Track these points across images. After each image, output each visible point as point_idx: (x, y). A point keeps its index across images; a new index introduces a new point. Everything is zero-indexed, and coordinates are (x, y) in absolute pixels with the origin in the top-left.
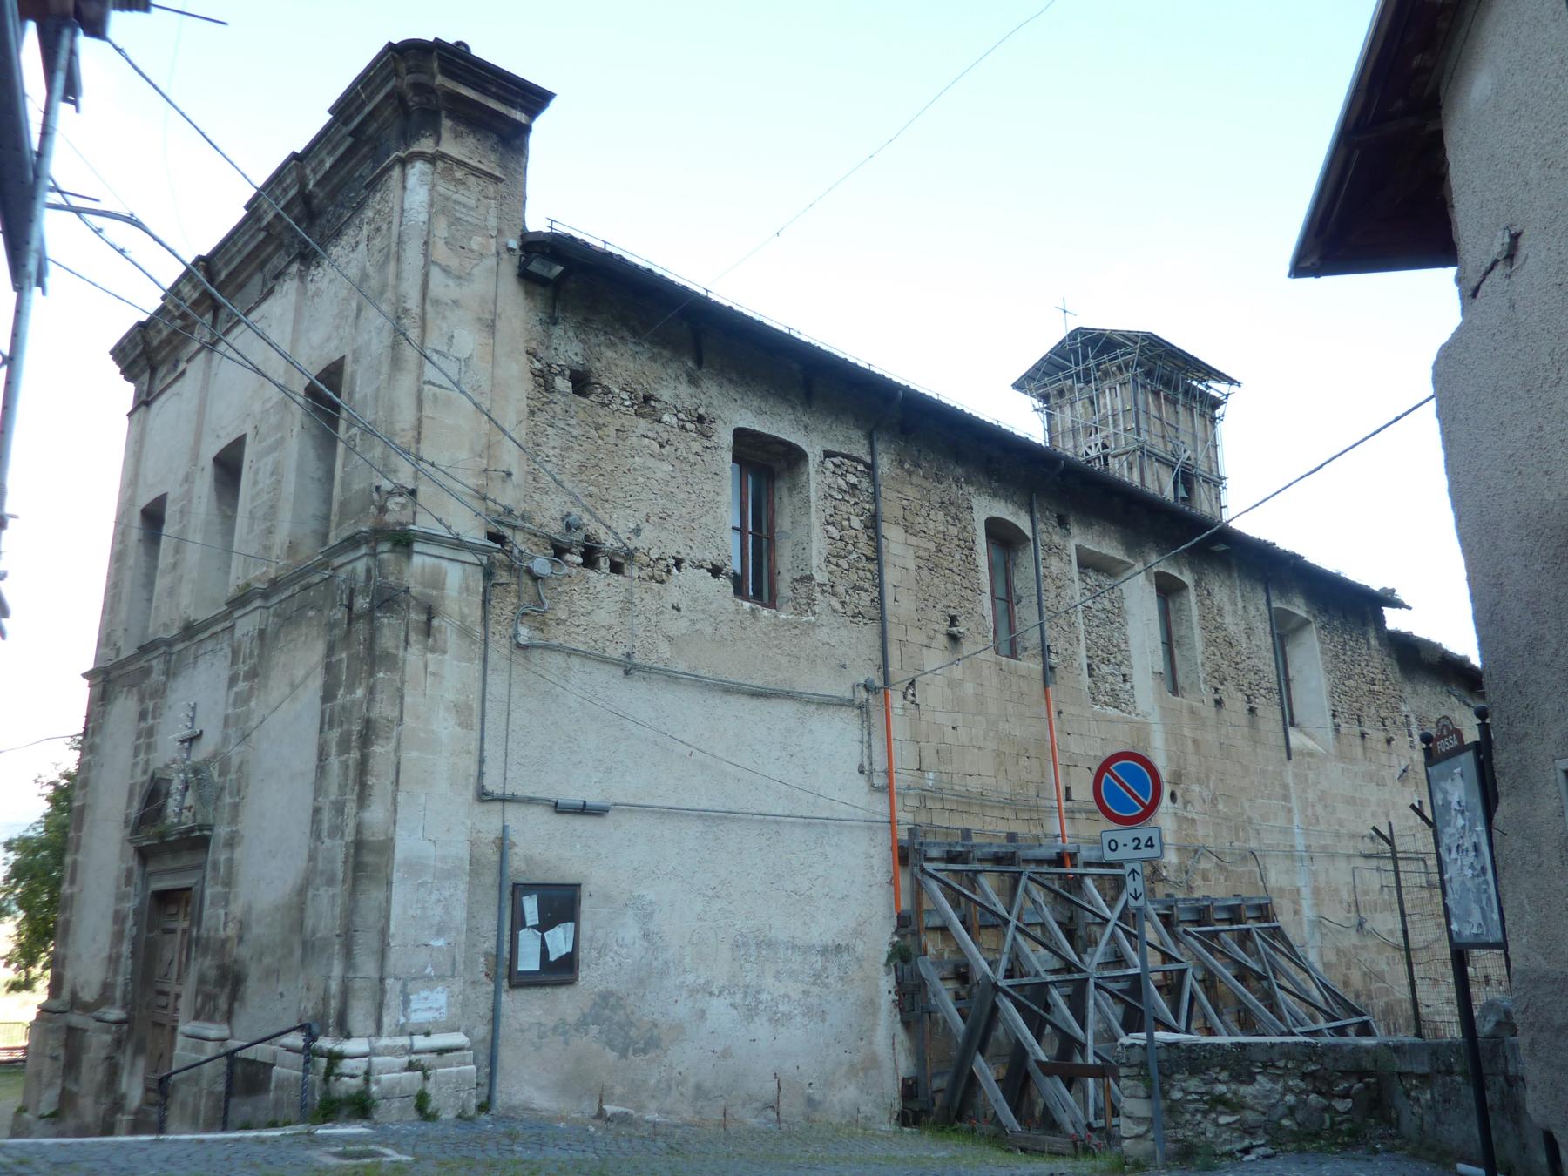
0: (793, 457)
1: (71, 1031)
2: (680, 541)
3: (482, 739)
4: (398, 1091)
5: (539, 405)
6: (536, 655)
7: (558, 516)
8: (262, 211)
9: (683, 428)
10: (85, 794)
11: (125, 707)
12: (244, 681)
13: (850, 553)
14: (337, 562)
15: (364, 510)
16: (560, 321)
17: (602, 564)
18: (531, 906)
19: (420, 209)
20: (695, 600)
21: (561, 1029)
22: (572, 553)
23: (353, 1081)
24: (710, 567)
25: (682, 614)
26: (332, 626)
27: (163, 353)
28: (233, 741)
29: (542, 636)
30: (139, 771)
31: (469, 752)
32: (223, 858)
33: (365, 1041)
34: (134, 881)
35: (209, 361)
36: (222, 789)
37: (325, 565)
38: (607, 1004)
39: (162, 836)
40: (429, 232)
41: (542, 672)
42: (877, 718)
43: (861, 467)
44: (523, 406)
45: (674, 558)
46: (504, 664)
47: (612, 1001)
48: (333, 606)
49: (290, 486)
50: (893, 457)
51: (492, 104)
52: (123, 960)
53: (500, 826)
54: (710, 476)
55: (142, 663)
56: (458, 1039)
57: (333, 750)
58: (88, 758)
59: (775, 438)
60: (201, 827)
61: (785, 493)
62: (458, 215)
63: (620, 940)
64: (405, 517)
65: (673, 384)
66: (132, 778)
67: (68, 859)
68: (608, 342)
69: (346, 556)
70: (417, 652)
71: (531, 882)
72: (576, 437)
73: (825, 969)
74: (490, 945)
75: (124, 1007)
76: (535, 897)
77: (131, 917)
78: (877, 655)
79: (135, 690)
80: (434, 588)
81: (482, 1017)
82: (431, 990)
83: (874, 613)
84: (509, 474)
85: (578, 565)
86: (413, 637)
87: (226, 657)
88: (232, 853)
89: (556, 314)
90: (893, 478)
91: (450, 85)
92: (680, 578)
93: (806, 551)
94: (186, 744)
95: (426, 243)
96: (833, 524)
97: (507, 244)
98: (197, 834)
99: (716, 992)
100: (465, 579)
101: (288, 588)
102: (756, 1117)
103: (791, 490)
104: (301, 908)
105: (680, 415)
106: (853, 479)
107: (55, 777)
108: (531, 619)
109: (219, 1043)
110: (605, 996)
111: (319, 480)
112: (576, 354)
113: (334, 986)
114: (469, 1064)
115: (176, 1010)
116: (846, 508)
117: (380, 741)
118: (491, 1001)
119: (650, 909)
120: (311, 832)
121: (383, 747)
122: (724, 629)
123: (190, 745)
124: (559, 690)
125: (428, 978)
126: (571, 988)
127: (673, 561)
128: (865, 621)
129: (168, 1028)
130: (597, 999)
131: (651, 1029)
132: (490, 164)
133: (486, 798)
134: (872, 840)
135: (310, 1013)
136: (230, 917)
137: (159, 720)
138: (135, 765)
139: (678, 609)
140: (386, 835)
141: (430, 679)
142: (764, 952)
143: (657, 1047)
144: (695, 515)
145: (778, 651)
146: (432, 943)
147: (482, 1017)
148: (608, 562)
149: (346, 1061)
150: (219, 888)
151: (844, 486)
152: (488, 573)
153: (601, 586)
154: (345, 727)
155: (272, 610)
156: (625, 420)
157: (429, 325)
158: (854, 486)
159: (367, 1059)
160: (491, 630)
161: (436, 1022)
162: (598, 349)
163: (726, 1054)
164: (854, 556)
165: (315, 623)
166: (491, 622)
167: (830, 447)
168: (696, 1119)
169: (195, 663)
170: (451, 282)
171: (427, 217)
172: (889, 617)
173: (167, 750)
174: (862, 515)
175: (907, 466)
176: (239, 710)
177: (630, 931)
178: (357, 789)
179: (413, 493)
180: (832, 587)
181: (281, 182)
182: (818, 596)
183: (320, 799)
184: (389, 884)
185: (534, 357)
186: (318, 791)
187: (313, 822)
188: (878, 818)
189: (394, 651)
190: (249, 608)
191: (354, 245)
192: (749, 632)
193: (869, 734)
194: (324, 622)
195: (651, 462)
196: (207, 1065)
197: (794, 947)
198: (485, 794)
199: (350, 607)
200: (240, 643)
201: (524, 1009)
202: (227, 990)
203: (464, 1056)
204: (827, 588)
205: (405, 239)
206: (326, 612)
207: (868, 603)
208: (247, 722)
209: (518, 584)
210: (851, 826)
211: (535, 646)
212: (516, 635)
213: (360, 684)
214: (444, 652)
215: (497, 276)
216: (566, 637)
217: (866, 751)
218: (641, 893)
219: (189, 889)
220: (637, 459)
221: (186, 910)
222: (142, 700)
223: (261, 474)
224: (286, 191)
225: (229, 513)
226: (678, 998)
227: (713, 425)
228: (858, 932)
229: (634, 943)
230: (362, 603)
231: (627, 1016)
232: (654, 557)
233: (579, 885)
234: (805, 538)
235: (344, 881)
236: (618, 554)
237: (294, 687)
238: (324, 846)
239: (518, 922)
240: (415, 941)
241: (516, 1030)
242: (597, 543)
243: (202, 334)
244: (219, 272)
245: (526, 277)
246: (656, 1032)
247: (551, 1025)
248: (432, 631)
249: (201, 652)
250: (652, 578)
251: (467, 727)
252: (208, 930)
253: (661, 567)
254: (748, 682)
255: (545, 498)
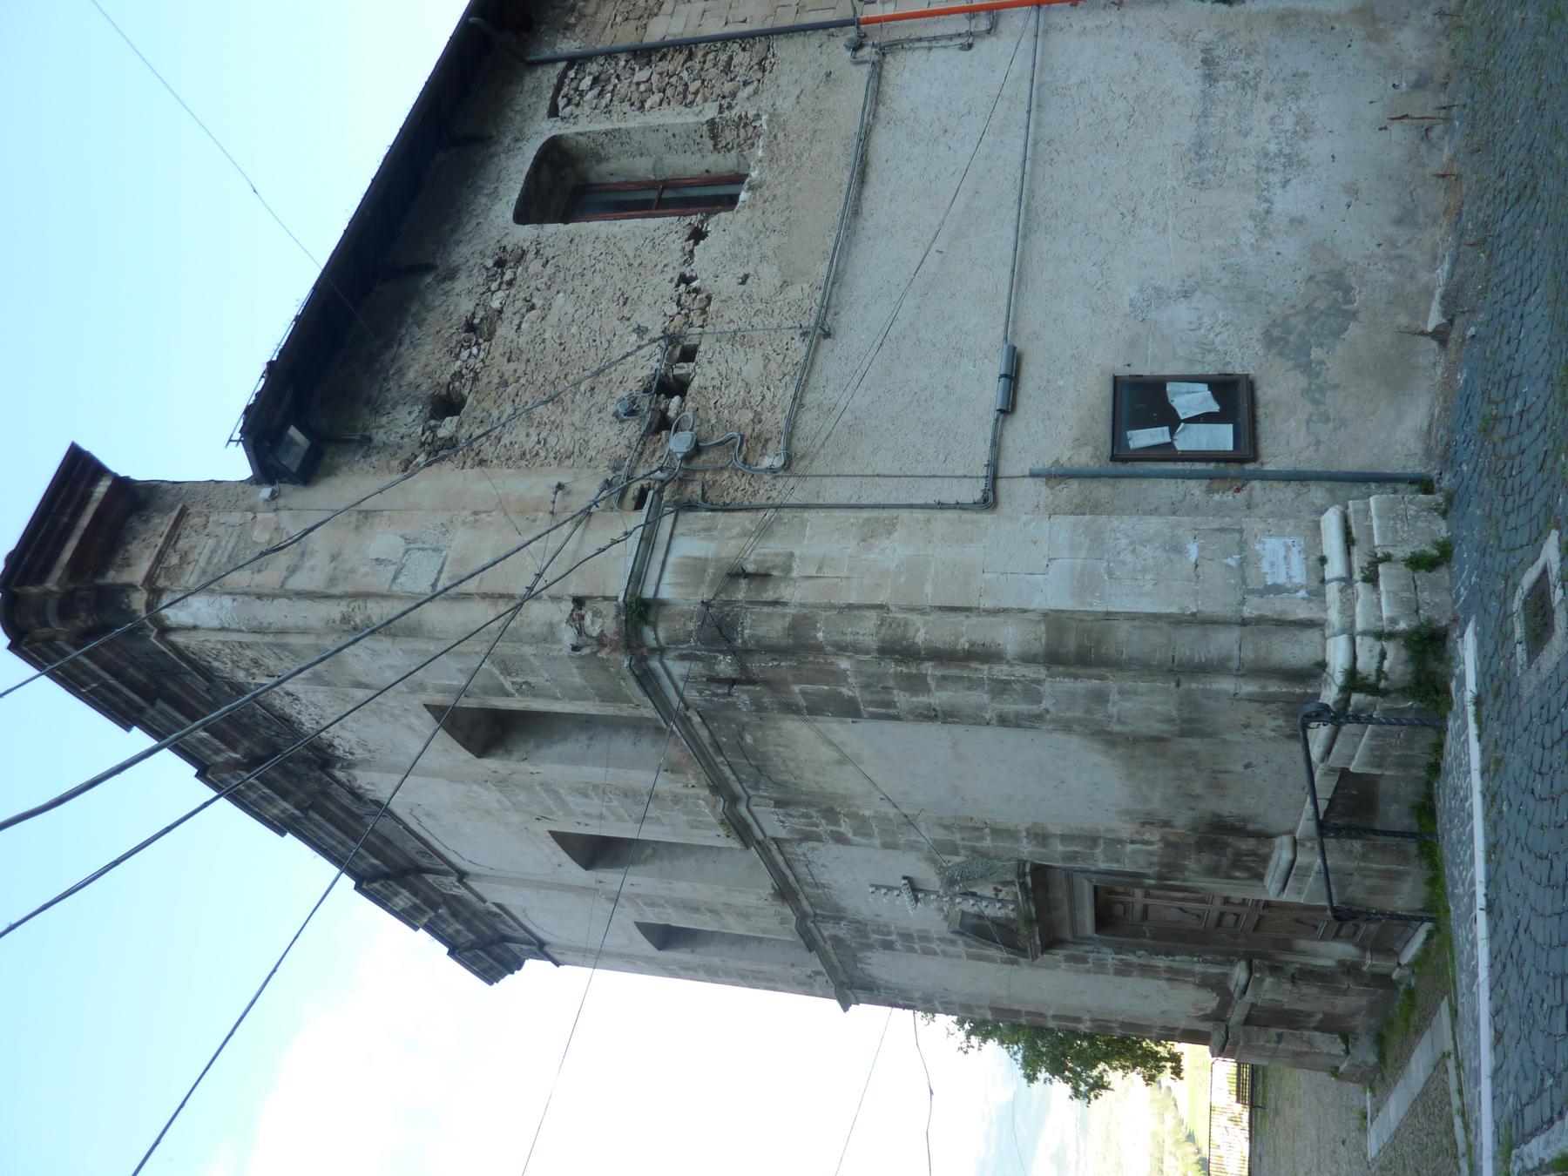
0: (555, 155)
1: (1248, 1021)
2: (656, 280)
3: (910, 506)
4: (1407, 594)
5: (472, 454)
6: (799, 445)
7: (617, 426)
8: (283, 816)
9: (510, 283)
10: (979, 1007)
11: (878, 965)
12: (840, 826)
13: (681, 79)
14: (675, 700)
15: (604, 666)
16: (367, 433)
17: (683, 372)
18: (1141, 438)
19: (217, 605)
20: (735, 257)
21: (1316, 392)
22: (667, 409)
23: (1390, 656)
24: (692, 242)
25: (752, 273)
26: (759, 708)
27: (483, 928)
28: (913, 838)
29: (774, 441)
30: (951, 949)
31: (928, 520)
32: (1060, 848)
33: (1330, 644)
34: (1082, 953)
35: (478, 876)
36: (974, 850)
37: (685, 720)
38: (1282, 339)
39: (1029, 922)
40: (246, 594)
41: (823, 436)
42: (899, 31)
43: (572, 74)
44: (472, 473)
45: (678, 286)
46: (811, 484)
47: (1276, 333)
48: (733, 706)
49: (595, 773)
50: (560, 36)
51: (85, 521)
52: (1175, 965)
53: (1030, 480)
54: (573, 249)
55: (828, 947)
56: (1331, 523)
57: (922, 699)
58: (937, 1004)
59: (529, 176)
60: (1021, 875)
61: (604, 168)
62: (224, 559)
63: (1192, 327)
64: (609, 610)
65: (453, 299)
66: (959, 957)
67: (1051, 1024)
68: (396, 377)
69: (666, 690)
70: (790, 590)
71: (1109, 439)
72: (516, 410)
73: (1235, 77)
74: (1196, 488)
75: (1232, 964)
76: (1130, 433)
77: (1124, 957)
78: (816, 38)
79: (860, 955)
80: (704, 571)
81: (1299, 495)
82: (1259, 558)
83: (759, 47)
84: (560, 487)
85: (683, 401)
86: (770, 595)
87: (814, 849)
88: (1055, 835)
89: (358, 438)
90: (586, 36)
91: (57, 572)
92: (704, 277)
93: (677, 132)
94: (920, 895)
95: (260, 597)
96: (643, 102)
97: (266, 500)
98: (1029, 879)
99: (1266, 205)
100: (693, 533)
101: (721, 771)
102: (1441, 150)
103: (600, 159)
104: (1134, 741)
105: (493, 288)
106: (588, 81)
107: (962, 1035)
108: (752, 453)
109: (1298, 847)
110: (1270, 341)
111: (591, 738)
112: (410, 413)
113: (1249, 687)
114: (1368, 504)
115: (1244, 902)
116: (623, 88)
117: (910, 634)
118: (1275, 484)
119: (1150, 291)
120: (1033, 727)
121: (918, 630)
122: (774, 221)
123: (921, 890)
124: (847, 416)
125: (1243, 562)
126: (1258, 384)
127: (683, 286)
128: (770, 56)
129: (1265, 913)
130: (1273, 351)
131: (1317, 283)
132: (163, 524)
133: (991, 499)
134: (1061, 29)
135: (1280, 722)
136: (1136, 837)
137: (893, 928)
138: (945, 954)
139: (746, 277)
140: (1038, 622)
141: (827, 572)
142: (1211, 151)
143: (1341, 274)
144: (624, 263)
145: (806, 155)
146: (1193, 558)
147: (1299, 495)
148: (680, 364)
149: (1360, 665)
150: (1098, 851)
151: (596, 91)
152: (691, 507)
153: (711, 372)
154: (891, 683)
155: (752, 793)
156: (497, 352)
157: (361, 588)
158: (596, 80)
159: (1358, 639)
160: (764, 502)
161: (1306, 551)
162: (405, 388)
163: (1352, 190)
164: (685, 74)
165: (760, 734)
166: (754, 503)
167: (545, 111)
168: (1444, 222)
169: (823, 886)
170: (308, 564)
171: (227, 596)
172: (768, 25)
173: (927, 917)
174: (633, 70)
175: (573, 20)
176: (876, 830)
177: (1181, 314)
178: (974, 665)
179: (579, 602)
180: (724, 97)
181: (239, 792)
182: (735, 112)
183: (988, 717)
184: (1109, 616)
185: (411, 463)
186: (975, 719)
187: (1018, 726)
188: (1032, 23)
189: (788, 619)
190: (750, 820)
191: (291, 698)
192: (779, 191)
193: (920, 40)
194: (756, 720)
195: (553, 318)
196: (1328, 862)
197: (1205, 114)
198: (985, 500)
199: (733, 682)
200: (793, 831)
201: (1277, 453)
202: (1230, 840)
203: (1356, 512)
204: (725, 103)
205: (255, 623)
206: (745, 719)
207: (747, 54)
208: (890, 820)
209: (705, 471)
210: (1043, 54)
211: (788, 447)
212: (771, 469)
213: (832, 663)
214: (791, 555)
215: (304, 510)
216: (778, 410)
217: (942, 43)
218: (1126, 303)
219: (1096, 888)
220: (547, 336)
221: (1122, 894)
222: (870, 947)
223: (589, 811)
224: (250, 787)
225: (649, 851)
226: (1274, 251)
227: (509, 248)
228: (1187, 40)
229: (1196, 309)
230: (725, 666)
231: (1297, 313)
232: (675, 309)
233: (1116, 379)
234: (660, 136)
235: (1102, 678)
236: (670, 354)
237: (844, 760)
238: (1052, 710)
239: (1165, 453)
240: (1190, 581)
241: (1317, 450)
242: (654, 379)
243: (449, 884)
244: (372, 866)
245: (309, 472)
246: (1320, 277)
247: (1309, 408)
248: (762, 571)
249: (809, 879)
250: (703, 311)
251: (894, 525)
252: (1151, 864)
253: (690, 300)
254: (845, 187)
255: (593, 443)
